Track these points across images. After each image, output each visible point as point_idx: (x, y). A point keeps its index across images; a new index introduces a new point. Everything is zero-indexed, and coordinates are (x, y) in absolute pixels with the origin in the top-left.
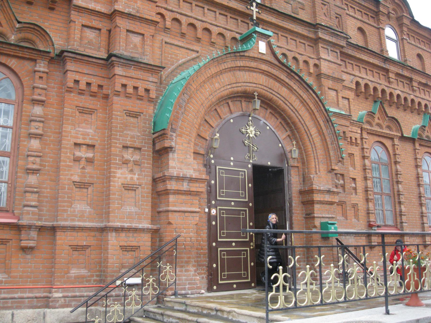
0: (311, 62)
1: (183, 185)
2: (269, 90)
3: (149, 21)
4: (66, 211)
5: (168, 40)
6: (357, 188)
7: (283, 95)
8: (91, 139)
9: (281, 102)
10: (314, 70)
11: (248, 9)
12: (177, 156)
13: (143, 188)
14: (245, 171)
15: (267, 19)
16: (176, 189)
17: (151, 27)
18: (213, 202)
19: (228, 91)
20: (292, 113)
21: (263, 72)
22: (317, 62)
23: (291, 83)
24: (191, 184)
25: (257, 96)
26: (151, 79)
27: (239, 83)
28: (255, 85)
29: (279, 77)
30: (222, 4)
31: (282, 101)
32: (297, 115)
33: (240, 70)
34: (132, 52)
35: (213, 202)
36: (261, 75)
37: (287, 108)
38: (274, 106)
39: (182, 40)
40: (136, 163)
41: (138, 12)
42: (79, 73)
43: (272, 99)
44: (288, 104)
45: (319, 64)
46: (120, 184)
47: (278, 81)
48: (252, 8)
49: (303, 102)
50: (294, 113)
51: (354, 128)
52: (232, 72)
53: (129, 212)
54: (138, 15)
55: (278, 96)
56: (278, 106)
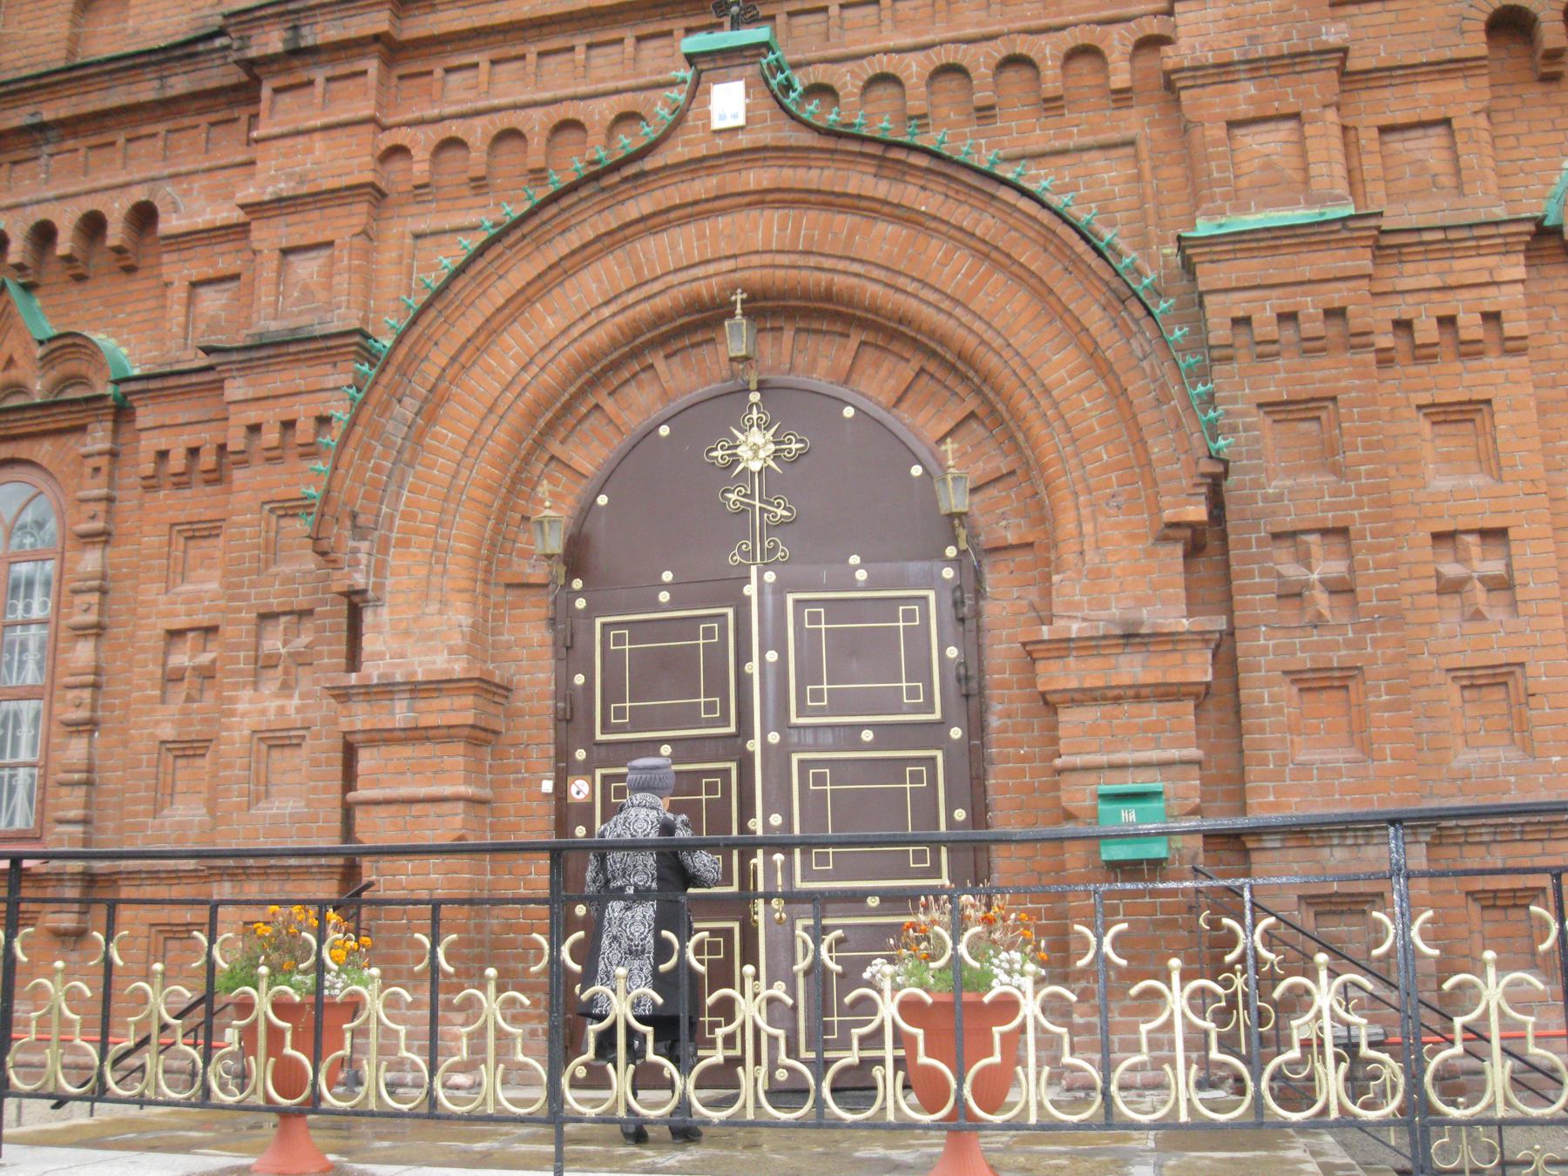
0: (1117, 43)
1: (392, 713)
2: (800, 260)
3: (1312, 58)
4: (142, 827)
5: (423, 226)
6: (1518, 577)
8: (207, 610)
9: (872, 288)
12: (391, 613)
13: (316, 737)
14: (604, 625)
16: (367, 727)
17: (353, 208)
18: (581, 755)
20: (942, 318)
21: (761, 199)
22: (1154, 27)
24: (421, 704)
26: (330, 382)
27: (655, 279)
28: (730, 264)
29: (836, 189)
31: (877, 281)
32: (967, 319)
33: (654, 231)
34: (301, 313)
35: (581, 755)
36: (755, 213)
37: (913, 304)
38: (859, 313)
39: (480, 200)
40: (300, 660)
41: (301, 182)
42: (166, 430)
44: (911, 287)
45: (1166, 32)
46: (247, 732)
47: (843, 206)
49: (986, 256)
50: (950, 315)
51: (1458, 265)
52: (618, 252)
53: (274, 816)
54: (305, 189)
55: (856, 268)
56: (875, 310)
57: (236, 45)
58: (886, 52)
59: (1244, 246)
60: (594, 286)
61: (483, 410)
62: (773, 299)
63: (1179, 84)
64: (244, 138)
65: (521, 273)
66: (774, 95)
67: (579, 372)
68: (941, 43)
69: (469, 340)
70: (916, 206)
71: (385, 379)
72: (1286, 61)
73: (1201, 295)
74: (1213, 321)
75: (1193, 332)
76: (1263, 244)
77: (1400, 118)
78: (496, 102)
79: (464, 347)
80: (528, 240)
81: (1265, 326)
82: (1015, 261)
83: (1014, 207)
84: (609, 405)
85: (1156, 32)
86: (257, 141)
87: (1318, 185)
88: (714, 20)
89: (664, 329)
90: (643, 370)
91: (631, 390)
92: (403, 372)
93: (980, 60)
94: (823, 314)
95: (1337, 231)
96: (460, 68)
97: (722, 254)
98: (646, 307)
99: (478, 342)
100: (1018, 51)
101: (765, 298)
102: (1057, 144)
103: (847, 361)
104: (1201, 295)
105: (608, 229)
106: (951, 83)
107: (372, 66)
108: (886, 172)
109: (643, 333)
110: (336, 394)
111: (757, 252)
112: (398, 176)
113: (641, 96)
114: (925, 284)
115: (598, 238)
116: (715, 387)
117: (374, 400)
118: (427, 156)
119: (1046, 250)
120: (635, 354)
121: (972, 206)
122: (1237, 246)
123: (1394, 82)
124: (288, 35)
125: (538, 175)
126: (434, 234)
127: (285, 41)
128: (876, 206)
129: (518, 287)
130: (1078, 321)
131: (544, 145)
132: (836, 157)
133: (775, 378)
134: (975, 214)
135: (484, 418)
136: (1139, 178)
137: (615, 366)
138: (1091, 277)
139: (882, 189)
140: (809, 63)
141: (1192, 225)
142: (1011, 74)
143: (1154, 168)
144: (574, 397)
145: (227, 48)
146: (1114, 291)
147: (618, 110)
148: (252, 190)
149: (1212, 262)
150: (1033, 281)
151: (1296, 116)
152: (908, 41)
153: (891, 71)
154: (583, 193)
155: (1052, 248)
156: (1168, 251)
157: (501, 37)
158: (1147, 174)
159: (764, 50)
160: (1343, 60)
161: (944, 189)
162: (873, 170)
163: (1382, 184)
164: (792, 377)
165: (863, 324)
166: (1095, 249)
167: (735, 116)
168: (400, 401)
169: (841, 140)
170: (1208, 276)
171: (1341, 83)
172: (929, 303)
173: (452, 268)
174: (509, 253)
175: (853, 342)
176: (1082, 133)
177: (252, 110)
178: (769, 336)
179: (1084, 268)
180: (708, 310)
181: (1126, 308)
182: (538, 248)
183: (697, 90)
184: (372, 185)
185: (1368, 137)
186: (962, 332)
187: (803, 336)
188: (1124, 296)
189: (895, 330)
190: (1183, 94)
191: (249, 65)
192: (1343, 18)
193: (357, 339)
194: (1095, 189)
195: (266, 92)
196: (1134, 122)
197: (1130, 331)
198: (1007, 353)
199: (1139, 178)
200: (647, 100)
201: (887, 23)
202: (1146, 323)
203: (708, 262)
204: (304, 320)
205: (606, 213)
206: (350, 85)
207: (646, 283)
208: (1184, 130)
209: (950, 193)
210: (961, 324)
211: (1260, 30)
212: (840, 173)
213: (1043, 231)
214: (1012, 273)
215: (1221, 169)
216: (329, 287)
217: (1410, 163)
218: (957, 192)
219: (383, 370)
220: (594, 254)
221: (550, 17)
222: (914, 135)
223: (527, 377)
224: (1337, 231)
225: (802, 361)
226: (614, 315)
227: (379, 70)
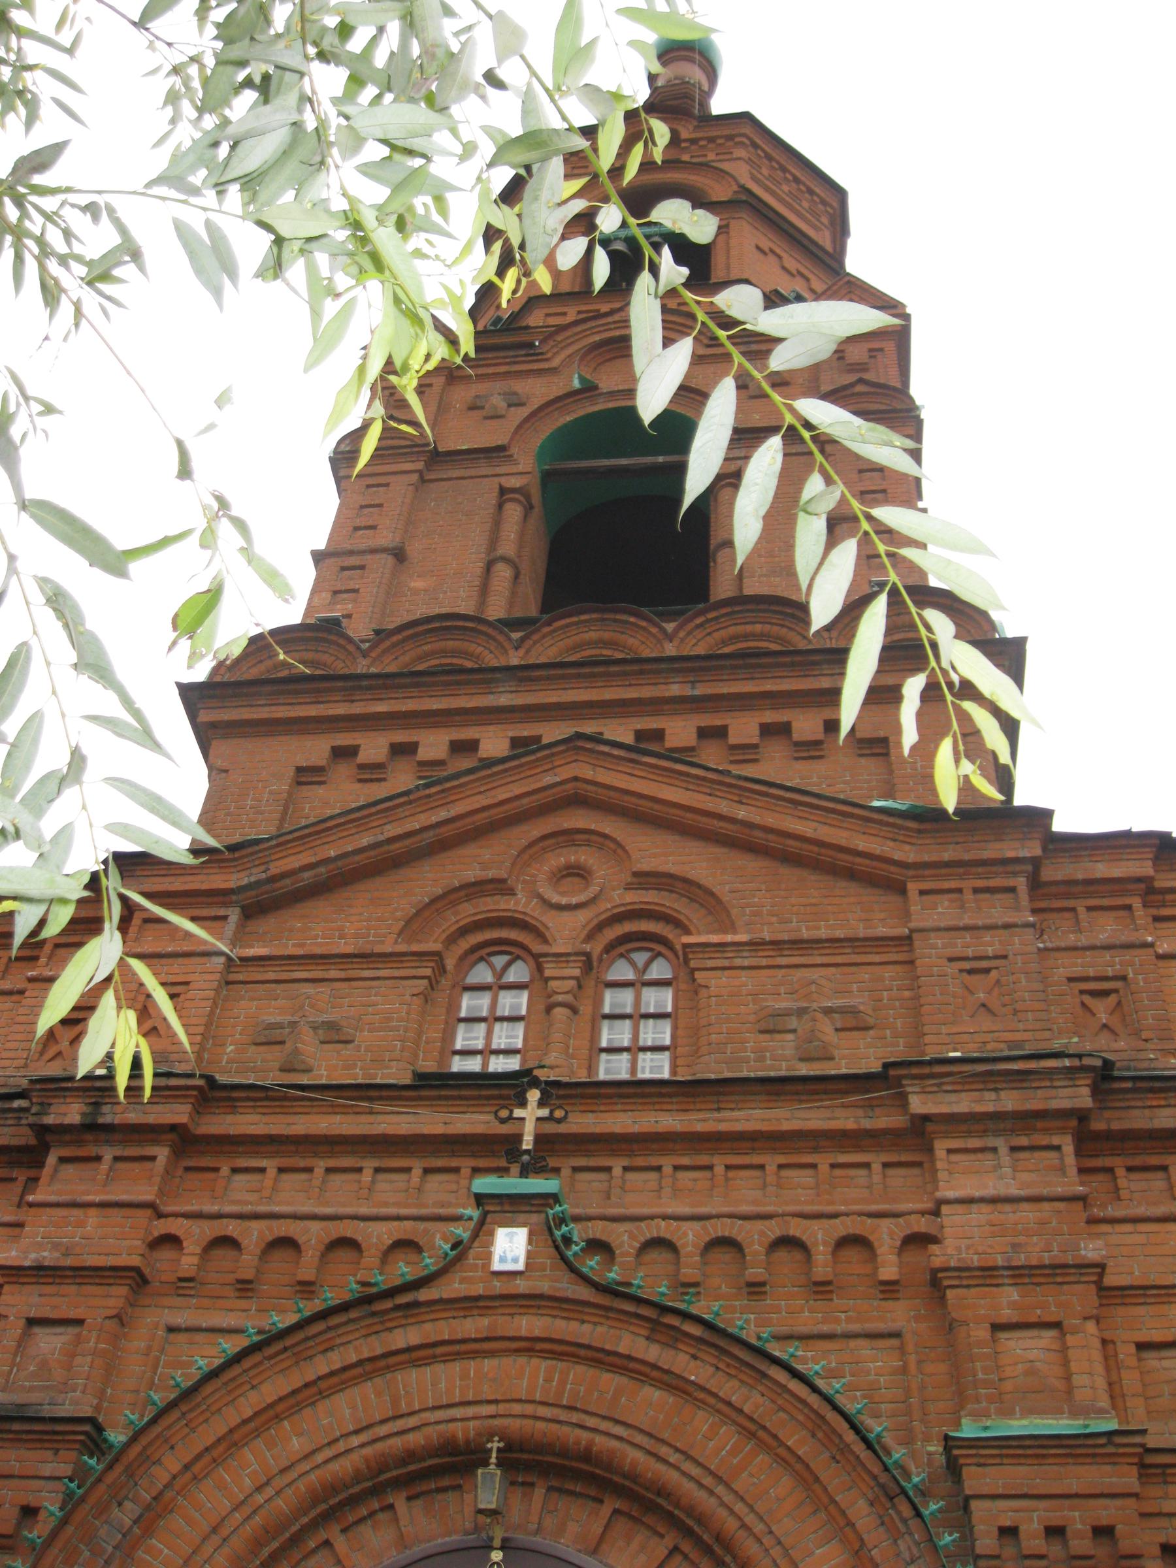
0: (886, 1235)
2: (563, 1415)
3: (1073, 1271)
5: (179, 1320)
7: (643, 1422)
10: (901, 1265)
11: (503, 1121)
15: (636, 1129)
17: (115, 1290)
19: (355, 1456)
20: (700, 1494)
21: (531, 1346)
22: (922, 1225)
23: (679, 1361)
25: (499, 1450)
26: (47, 1470)
28: (486, 1410)
29: (607, 1347)
30: (424, 1136)
32: (728, 1498)
33: (417, 1363)
34: (31, 1389)
36: (522, 1360)
38: (615, 1478)
39: (243, 1304)
43: (588, 1449)
44: (674, 1458)
45: (933, 1231)
48: (518, 1113)
49: (753, 1435)
50: (711, 1493)
54: (68, 1262)
55: (618, 1430)
56: (633, 1476)
57: (34, 1110)
58: (665, 1217)
59: (1011, 1452)
60: (347, 1411)
61: (206, 1527)
62: (529, 1452)
63: (946, 1283)
64: (17, 1199)
65: (275, 1387)
66: (551, 1242)
67: (316, 1500)
68: (718, 1216)
69: (207, 1449)
70: (685, 1374)
71: (110, 1478)
72: (1047, 1272)
73: (967, 1499)
74: (979, 1528)
75: (963, 1537)
76: (1029, 1452)
77: (1157, 1336)
78: (276, 1209)
79: (199, 1457)
80: (289, 1353)
81: (1033, 1539)
82: (782, 1444)
83: (783, 1387)
84: (341, 1543)
85: (923, 1230)
86: (31, 1205)
87: (1082, 1395)
88: (503, 1163)
89: (412, 1467)
90: (382, 1509)
91: (366, 1530)
92: (130, 1472)
93: (755, 1237)
94: (577, 1475)
95: (1102, 1446)
96: (246, 1170)
97: (484, 1397)
98: (397, 1442)
99: (215, 1453)
100: (791, 1232)
101: (522, 1451)
102: (825, 1328)
103: (597, 1528)
104: (967, 1499)
105: (371, 1355)
106: (724, 1255)
107: (162, 1153)
108: (658, 1337)
109: (390, 1470)
110: (51, 1485)
111: (519, 1401)
112: (164, 1264)
113: (421, 1226)
114: (689, 1457)
115: (360, 1363)
116: (454, 1539)
117: (92, 1499)
118: (198, 1251)
119: (814, 1435)
120: (377, 1491)
121: (741, 1381)
122: (1005, 1451)
123: (1148, 1300)
124: (85, 1109)
125: (306, 1288)
126: (188, 1330)
127: (83, 1114)
128: (647, 1370)
129: (269, 1401)
130: (843, 1513)
131: (316, 1259)
132: (610, 1315)
133: (520, 1537)
134: (745, 1390)
135: (205, 1538)
136: (904, 1370)
137: (353, 1501)
138: (859, 1469)
139: (654, 1353)
140: (589, 1218)
141: (958, 1425)
142: (782, 1254)
143: (919, 1362)
144: (304, 1529)
145: (26, 1110)
146: (882, 1487)
147: (397, 1236)
148: (14, 1253)
149: (979, 1465)
150: (798, 1466)
151: (1057, 1325)
152: (687, 1210)
153: (668, 1236)
154: (353, 1314)
155: (820, 1435)
156: (931, 1449)
157: (293, 1148)
158: (912, 1367)
159: (551, 1201)
160: (1101, 1275)
161: (715, 1362)
162: (645, 1332)
163: (1142, 1399)
164: (538, 1539)
165: (619, 1491)
166: (865, 1440)
167: (515, 1260)
168: (120, 1504)
169: (616, 1297)
170: (975, 1479)
171: (1100, 1297)
172: (691, 1478)
173: (206, 1369)
174: (267, 1364)
175: (606, 1510)
176: (849, 1320)
177: (32, 1173)
178: (519, 1490)
179: (852, 1458)
180: (461, 1454)
181: (894, 1506)
182: (297, 1363)
183: (482, 1231)
184: (136, 1269)
185: (1126, 1352)
186: (722, 1512)
187: (555, 1495)
188: (891, 1491)
189: (651, 1501)
190: (948, 1292)
191: (42, 1130)
192: (1099, 1235)
193: (87, 1428)
194: (862, 1376)
195: (51, 1160)
196: (899, 1314)
197: (899, 1531)
198: (767, 1540)
199: (904, 1370)
200: (426, 1231)
201: (667, 1190)
202: (914, 1523)
203: (469, 1403)
204: (34, 1397)
205: (374, 1337)
206: (136, 1166)
207: (402, 1416)
208: (949, 1327)
209: (721, 1365)
210: (723, 1504)
211: (1021, 1239)
212: (612, 1331)
213: (813, 1416)
214: (776, 1454)
215: (985, 1370)
216: (69, 1367)
217: (1167, 1382)
218: (728, 1365)
219: (110, 1467)
220: (354, 1378)
221: (344, 1136)
222: (690, 1303)
223: (260, 1498)
224: (1102, 1446)
225: (549, 1522)
226: (362, 1445)
227: (168, 1158)
